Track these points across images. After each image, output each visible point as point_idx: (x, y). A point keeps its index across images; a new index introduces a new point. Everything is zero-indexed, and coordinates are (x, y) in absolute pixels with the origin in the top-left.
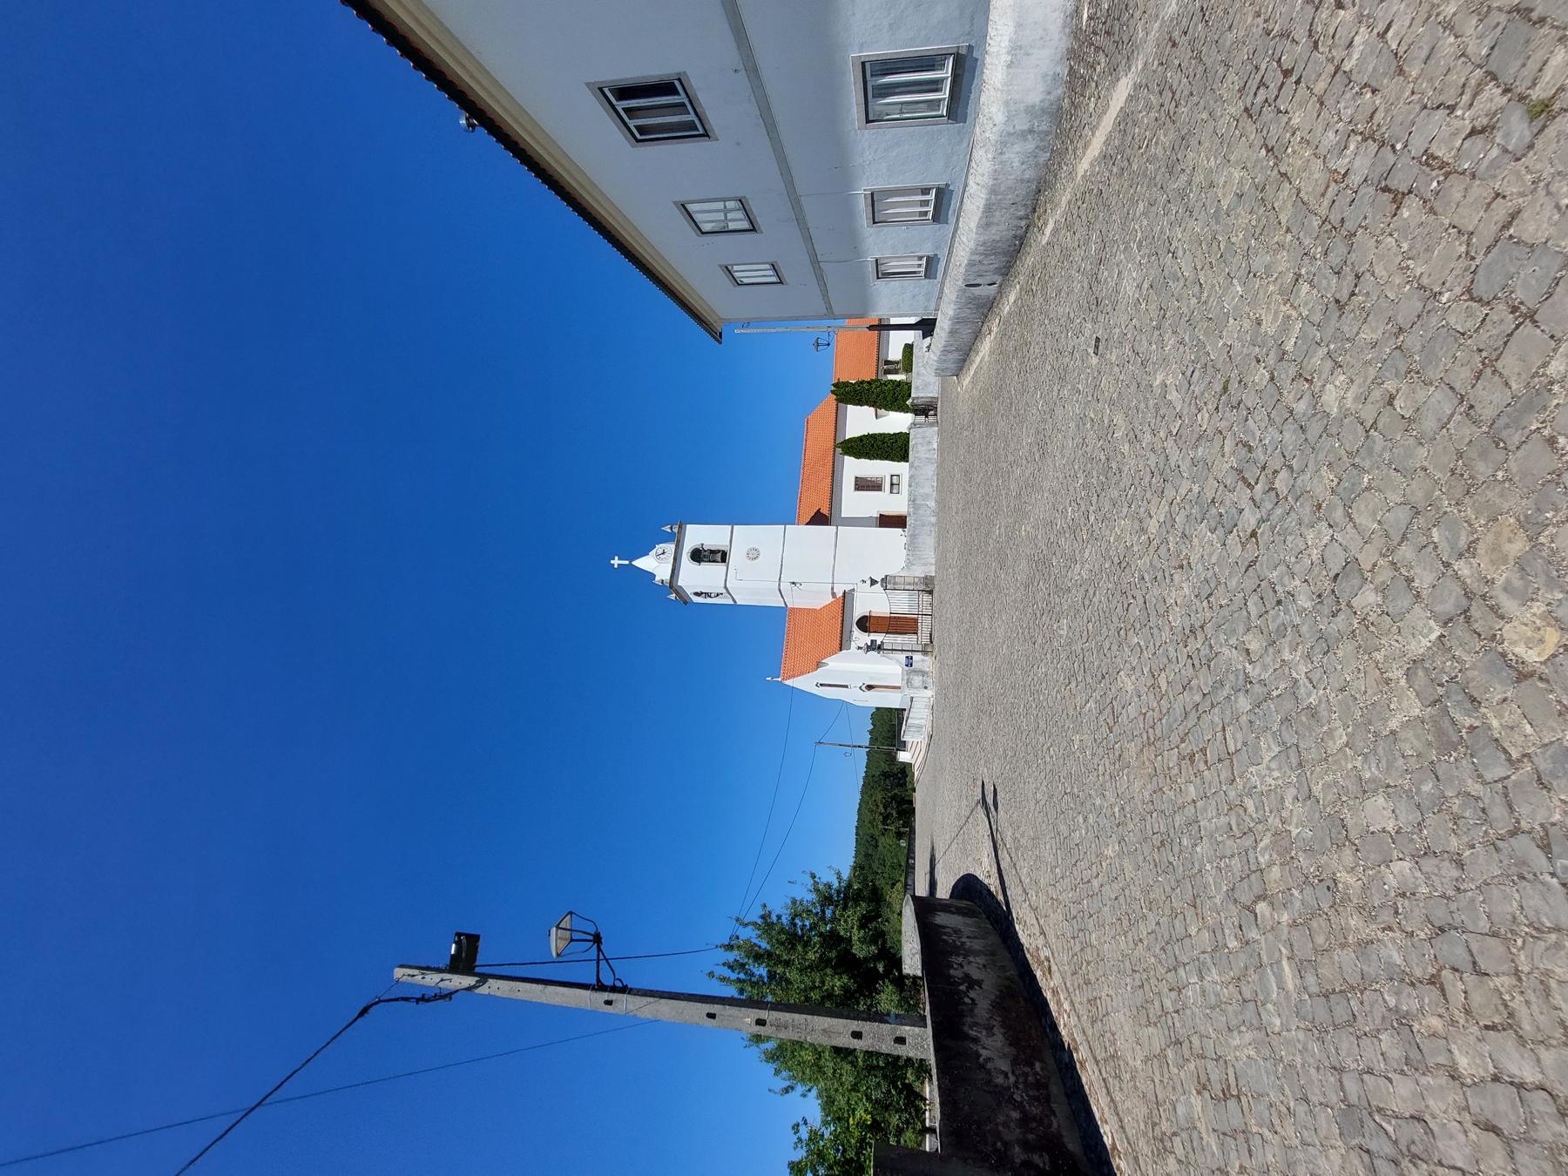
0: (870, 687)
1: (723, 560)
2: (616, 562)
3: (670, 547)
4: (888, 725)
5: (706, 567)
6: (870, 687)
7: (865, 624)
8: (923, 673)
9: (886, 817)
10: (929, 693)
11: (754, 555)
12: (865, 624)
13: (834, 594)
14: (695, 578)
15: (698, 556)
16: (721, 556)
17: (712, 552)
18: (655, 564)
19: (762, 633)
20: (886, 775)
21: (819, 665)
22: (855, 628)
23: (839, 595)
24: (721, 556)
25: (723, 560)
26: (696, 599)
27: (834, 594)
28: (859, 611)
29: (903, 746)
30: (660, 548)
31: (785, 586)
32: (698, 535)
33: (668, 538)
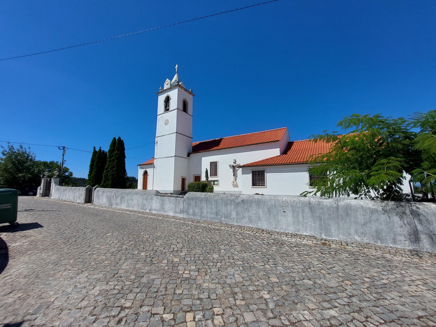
22: (145, 170)
26: (161, 99)
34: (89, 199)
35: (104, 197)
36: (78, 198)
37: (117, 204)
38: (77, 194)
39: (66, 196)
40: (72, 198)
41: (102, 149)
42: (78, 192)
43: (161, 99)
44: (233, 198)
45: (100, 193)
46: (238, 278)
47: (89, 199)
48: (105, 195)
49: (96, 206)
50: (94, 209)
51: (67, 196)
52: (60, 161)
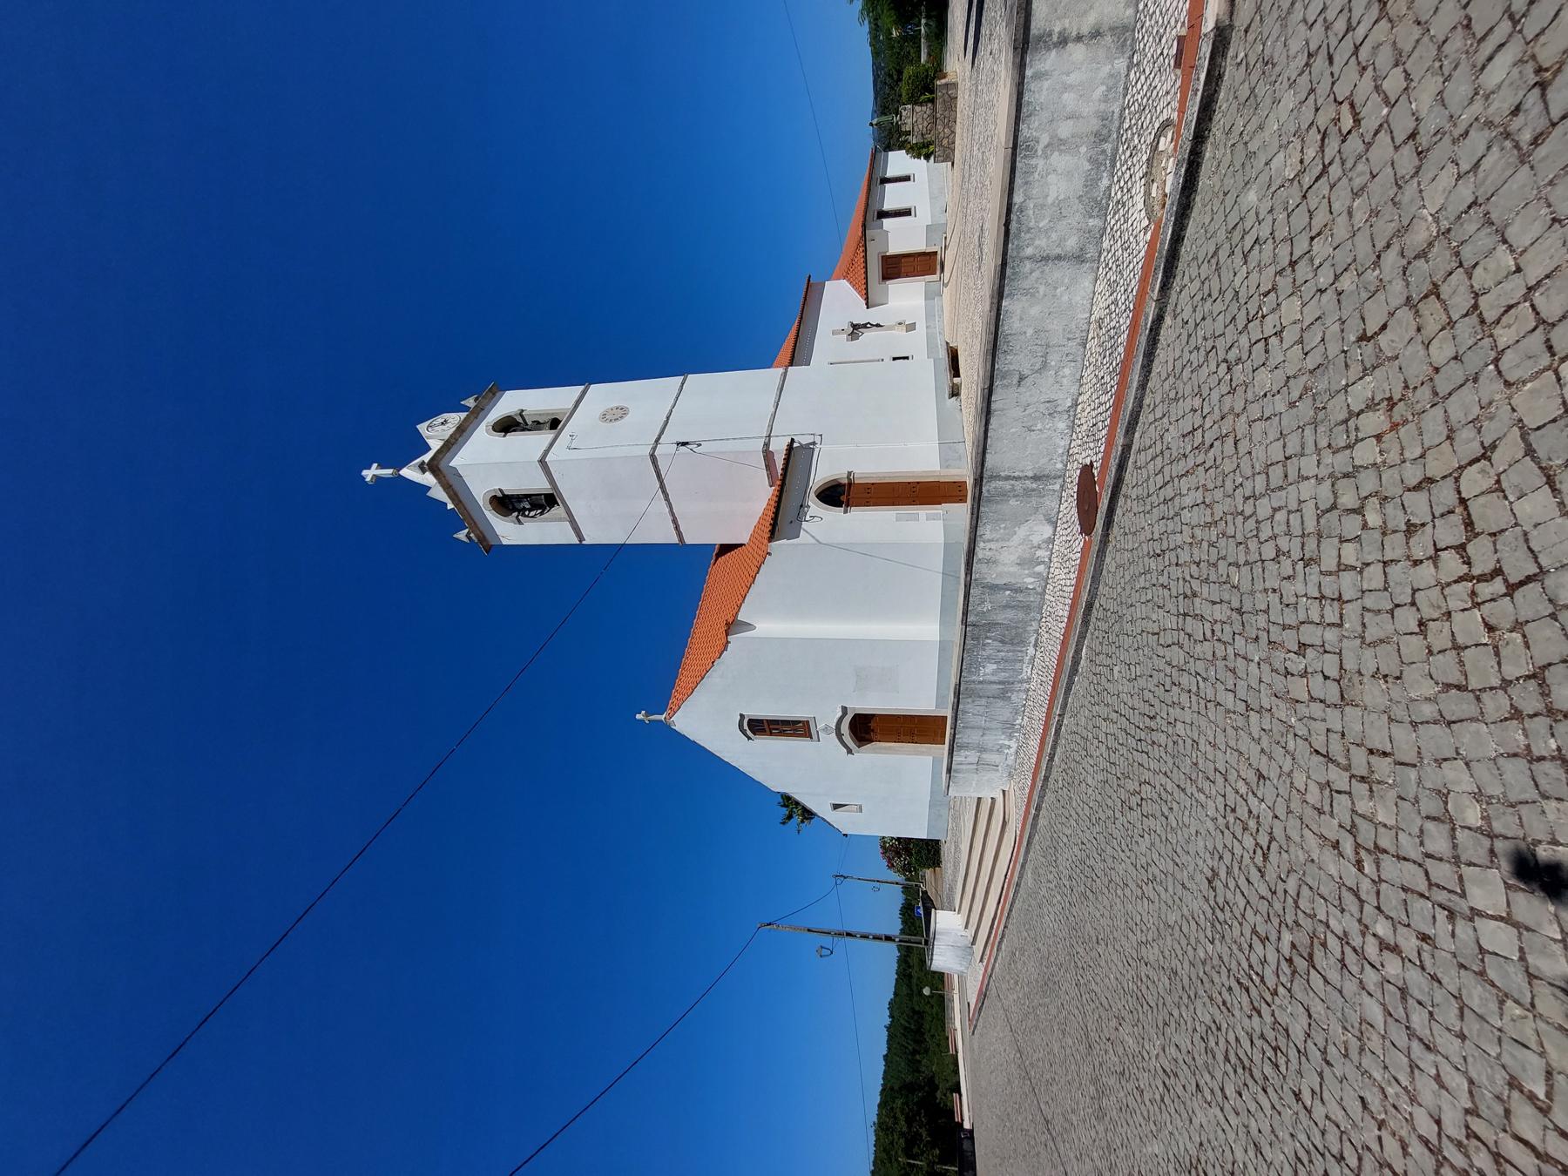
7: (835, 495)
9: (912, 1142)
12: (835, 495)
13: (768, 455)
15: (507, 426)
20: (908, 1088)
26: (508, 532)
27: (768, 455)
28: (824, 471)
30: (446, 416)
43: (508, 532)
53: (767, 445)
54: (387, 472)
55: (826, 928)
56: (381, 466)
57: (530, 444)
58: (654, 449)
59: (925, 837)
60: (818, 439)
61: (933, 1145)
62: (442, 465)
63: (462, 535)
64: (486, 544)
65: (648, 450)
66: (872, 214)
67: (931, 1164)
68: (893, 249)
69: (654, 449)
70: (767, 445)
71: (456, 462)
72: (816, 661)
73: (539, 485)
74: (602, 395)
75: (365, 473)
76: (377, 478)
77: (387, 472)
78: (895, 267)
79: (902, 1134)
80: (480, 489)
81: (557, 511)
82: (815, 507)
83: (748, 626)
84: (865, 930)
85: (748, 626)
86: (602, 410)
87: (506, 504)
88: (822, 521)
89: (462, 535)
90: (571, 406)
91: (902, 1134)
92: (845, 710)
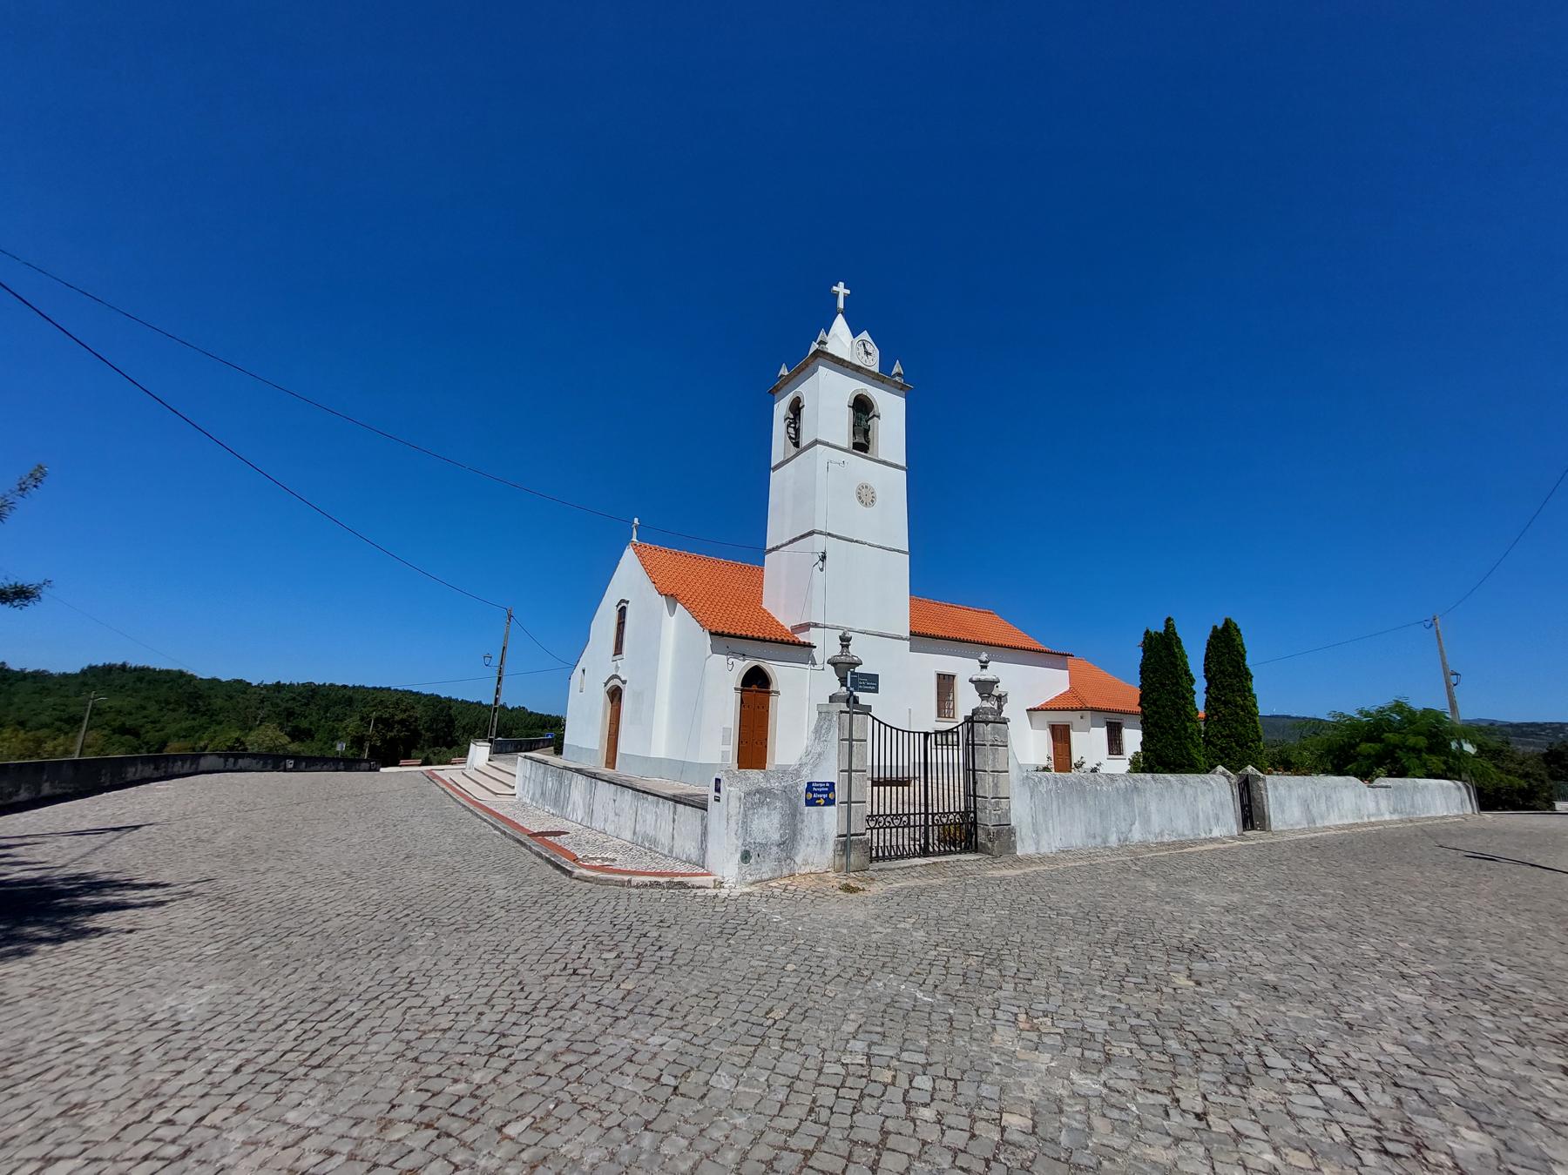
0: (615, 695)
1: (857, 446)
2: (841, 290)
3: (873, 363)
4: (532, 732)
5: (845, 417)
6: (615, 695)
7: (756, 682)
8: (788, 843)
9: (386, 723)
10: (726, 869)
11: (866, 496)
12: (756, 682)
13: (805, 627)
14: (826, 397)
15: (862, 406)
16: (862, 445)
17: (866, 432)
18: (840, 338)
19: (717, 515)
20: (451, 722)
21: (672, 598)
22: (749, 664)
23: (802, 637)
24: (862, 445)
25: (857, 446)
26: (781, 409)
27: (805, 627)
28: (781, 673)
29: (498, 750)
30: (876, 353)
31: (819, 543)
32: (891, 409)
33: (885, 364)
34: (1251, 814)
35: (1294, 803)
36: (1212, 821)
37: (1322, 818)
38: (1205, 804)
39: (1147, 821)
40: (1184, 827)
41: (1152, 631)
42: (1209, 797)
43: (781, 409)
44: (241, 762)
45: (1282, 791)
46: (672, 1044)
47: (1251, 814)
48: (1295, 794)
49: (1029, 861)
50: (1026, 882)
51: (1155, 818)
52: (1439, 703)
53: (816, 625)
54: (841, 305)
55: (506, 661)
56: (846, 297)
57: (839, 427)
58: (821, 533)
59: (566, 741)
60: (616, 682)
61: (384, 741)
62: (820, 360)
63: (784, 371)
64: (774, 392)
65: (818, 528)
66: (1115, 718)
67: (370, 738)
68: (1074, 735)
69: (821, 533)
70: (816, 625)
71: (823, 372)
72: (648, 667)
73: (805, 440)
74: (892, 486)
75: (841, 284)
76: (836, 295)
77: (841, 305)
78: (1061, 735)
79: (393, 716)
80: (805, 390)
81: (794, 450)
82: (742, 666)
83: (672, 611)
84: (502, 692)
85: (672, 611)
86: (871, 483)
87: (796, 408)
88: (728, 672)
89: (784, 371)
90: (881, 457)
91: (393, 716)
92: (624, 682)
